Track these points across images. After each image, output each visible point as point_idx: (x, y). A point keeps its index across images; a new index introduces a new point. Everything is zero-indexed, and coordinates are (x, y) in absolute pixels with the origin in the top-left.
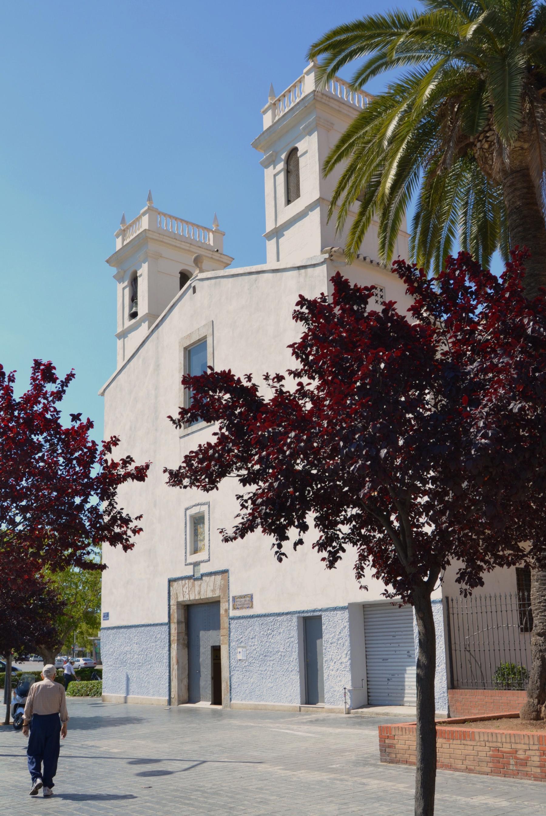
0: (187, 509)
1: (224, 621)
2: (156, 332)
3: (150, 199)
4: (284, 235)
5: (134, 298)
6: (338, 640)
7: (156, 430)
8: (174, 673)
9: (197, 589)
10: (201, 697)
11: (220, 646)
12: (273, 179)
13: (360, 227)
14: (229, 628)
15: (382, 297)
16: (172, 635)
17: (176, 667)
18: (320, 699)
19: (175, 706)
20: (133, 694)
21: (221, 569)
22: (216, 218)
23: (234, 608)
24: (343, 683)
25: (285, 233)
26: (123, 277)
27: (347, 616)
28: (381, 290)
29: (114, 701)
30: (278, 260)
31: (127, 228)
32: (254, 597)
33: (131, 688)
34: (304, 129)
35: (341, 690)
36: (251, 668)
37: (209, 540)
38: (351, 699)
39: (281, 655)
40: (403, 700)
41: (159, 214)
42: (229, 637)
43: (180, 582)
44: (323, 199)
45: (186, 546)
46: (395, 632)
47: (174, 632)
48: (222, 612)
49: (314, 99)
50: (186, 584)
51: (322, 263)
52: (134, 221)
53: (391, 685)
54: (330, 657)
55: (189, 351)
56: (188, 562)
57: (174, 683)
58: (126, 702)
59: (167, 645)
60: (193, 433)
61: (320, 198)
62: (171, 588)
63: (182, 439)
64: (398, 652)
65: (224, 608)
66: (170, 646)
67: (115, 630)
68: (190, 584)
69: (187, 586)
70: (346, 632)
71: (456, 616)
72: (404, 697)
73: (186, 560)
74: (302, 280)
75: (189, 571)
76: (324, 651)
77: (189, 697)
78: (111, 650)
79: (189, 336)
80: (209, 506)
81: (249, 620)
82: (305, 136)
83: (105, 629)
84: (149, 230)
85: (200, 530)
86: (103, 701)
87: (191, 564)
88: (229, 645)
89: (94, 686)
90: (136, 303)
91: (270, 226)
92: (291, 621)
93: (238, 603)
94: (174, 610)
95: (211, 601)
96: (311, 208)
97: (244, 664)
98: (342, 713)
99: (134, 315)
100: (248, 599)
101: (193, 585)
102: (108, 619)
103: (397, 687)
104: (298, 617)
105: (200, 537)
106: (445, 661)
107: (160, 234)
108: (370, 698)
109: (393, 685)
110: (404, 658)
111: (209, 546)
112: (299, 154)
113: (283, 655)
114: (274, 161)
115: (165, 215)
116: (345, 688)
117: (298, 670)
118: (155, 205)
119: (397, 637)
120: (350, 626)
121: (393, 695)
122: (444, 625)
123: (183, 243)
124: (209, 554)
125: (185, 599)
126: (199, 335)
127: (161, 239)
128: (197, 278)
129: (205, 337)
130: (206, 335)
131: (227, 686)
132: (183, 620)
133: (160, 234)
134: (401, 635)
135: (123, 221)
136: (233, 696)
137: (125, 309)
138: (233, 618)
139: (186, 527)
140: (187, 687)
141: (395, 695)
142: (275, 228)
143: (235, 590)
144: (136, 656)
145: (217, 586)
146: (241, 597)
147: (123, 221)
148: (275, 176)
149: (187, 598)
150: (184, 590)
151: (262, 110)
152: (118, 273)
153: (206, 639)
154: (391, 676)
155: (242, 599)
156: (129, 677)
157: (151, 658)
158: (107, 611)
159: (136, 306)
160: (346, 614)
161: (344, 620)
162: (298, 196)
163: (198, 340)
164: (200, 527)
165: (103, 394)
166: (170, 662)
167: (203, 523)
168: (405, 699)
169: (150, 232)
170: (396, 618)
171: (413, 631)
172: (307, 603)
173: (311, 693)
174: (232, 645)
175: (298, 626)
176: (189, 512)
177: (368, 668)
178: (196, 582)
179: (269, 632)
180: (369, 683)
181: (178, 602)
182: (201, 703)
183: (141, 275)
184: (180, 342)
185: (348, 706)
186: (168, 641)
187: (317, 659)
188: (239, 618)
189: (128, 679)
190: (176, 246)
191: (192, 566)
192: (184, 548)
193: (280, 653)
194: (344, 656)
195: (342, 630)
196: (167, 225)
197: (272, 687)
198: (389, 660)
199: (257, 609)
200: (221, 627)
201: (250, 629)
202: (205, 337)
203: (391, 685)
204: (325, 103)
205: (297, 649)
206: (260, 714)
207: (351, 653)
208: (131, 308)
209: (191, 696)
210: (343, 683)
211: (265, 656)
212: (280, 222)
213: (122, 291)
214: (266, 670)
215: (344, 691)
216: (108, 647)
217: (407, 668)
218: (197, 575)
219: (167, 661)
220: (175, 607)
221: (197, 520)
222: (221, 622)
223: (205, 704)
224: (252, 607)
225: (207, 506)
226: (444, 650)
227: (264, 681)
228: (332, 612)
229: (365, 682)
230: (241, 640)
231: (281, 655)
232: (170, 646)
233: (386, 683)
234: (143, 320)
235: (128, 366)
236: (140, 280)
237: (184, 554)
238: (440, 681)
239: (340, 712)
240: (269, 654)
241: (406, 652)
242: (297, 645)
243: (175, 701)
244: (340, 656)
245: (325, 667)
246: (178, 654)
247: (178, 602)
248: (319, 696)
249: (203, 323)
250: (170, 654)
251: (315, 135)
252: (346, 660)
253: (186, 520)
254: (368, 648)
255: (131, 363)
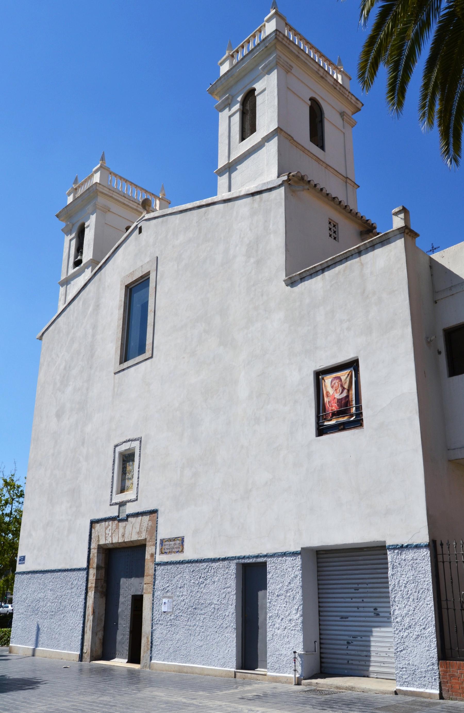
0: (116, 446)
1: (149, 567)
2: (99, 274)
3: (103, 159)
4: (237, 169)
5: (79, 249)
6: (287, 591)
7: (91, 368)
8: (89, 624)
9: (121, 530)
10: (117, 653)
11: (142, 596)
12: (228, 121)
13: (376, 46)
14: (155, 575)
15: (335, 232)
16: (89, 581)
17: (91, 618)
18: (259, 664)
19: (86, 663)
20: (41, 647)
21: (149, 509)
22: (163, 188)
23: (162, 553)
24: (291, 645)
25: (238, 167)
26: (71, 230)
27: (300, 563)
28: (334, 226)
29: (21, 654)
30: (230, 190)
31: (79, 187)
32: (185, 540)
33: (41, 640)
34: (263, 68)
35: (289, 653)
36: (177, 622)
37: (138, 478)
38: (302, 666)
39: (214, 608)
40: (368, 670)
41: (110, 173)
42: (154, 585)
43: (103, 523)
44: (281, 130)
45: (112, 485)
46: (358, 584)
47: (92, 578)
48: (147, 556)
49: (276, 38)
50: (109, 525)
51: (280, 186)
52: (86, 179)
53: (352, 650)
54: (276, 612)
55: (131, 290)
56: (113, 501)
57: (88, 636)
58: (33, 655)
59: (84, 592)
60: (128, 368)
61: (278, 127)
62: (93, 530)
63: (116, 375)
64: (361, 609)
65: (150, 553)
66: (86, 593)
67: (30, 575)
68: (114, 525)
69: (110, 527)
70: (298, 582)
71: (447, 565)
72: (369, 666)
73: (111, 499)
74: (256, 205)
75: (114, 512)
76: (268, 604)
77: (103, 652)
78: (24, 596)
79: (132, 274)
80: (141, 442)
81: (178, 566)
82: (264, 75)
83: (19, 573)
84: (100, 184)
85: (129, 468)
86: (10, 652)
87: (116, 504)
88: (153, 595)
89: (5, 634)
90: (82, 253)
91: (222, 162)
92: (228, 568)
93: (167, 547)
94: (94, 554)
95: (135, 545)
96: (268, 139)
97: (168, 617)
98: (290, 683)
99: (77, 263)
100: (178, 542)
101: (117, 527)
102: (24, 563)
103: (359, 653)
104: (237, 564)
105: (128, 476)
106: (434, 622)
107: (110, 189)
108: (323, 665)
109: (354, 650)
110: (369, 617)
111: (138, 484)
112: (256, 93)
113: (216, 608)
114: (230, 104)
115: (116, 175)
116: (295, 652)
117: (235, 627)
118: (106, 165)
119: (360, 590)
120: (303, 575)
121: (354, 662)
122: (432, 575)
123: (131, 202)
124: (137, 493)
125: (107, 542)
126: (142, 272)
127: (111, 195)
128: (144, 219)
129: (148, 273)
130: (149, 272)
131: (148, 642)
132: (103, 566)
133: (110, 189)
134: (366, 588)
135: (76, 181)
136: (154, 654)
137: (70, 259)
138: (159, 564)
139: (114, 464)
140: (102, 641)
141: (357, 663)
142: (228, 163)
143: (164, 532)
144: (49, 604)
145: (144, 528)
146: (170, 540)
147: (76, 181)
148: (230, 117)
149: (109, 541)
150: (107, 532)
151: (220, 62)
152: (67, 225)
153: (127, 587)
154: (351, 638)
155: (171, 543)
156: (40, 626)
157: (65, 607)
158: (23, 555)
159: (82, 255)
160: (298, 561)
161: (295, 568)
162: (253, 130)
163: (141, 277)
164: (129, 465)
165: (41, 338)
166: (85, 612)
167: (133, 460)
168: (371, 669)
169: (101, 186)
170: (359, 567)
171: (388, 583)
172: (248, 548)
173: (250, 655)
174: (156, 594)
175: (237, 574)
176: (118, 449)
177: (322, 627)
178: (120, 524)
179: (201, 580)
180: (322, 646)
181: (99, 545)
182: (116, 660)
183: (88, 226)
184: (122, 281)
185: (297, 676)
186: (85, 588)
187: (257, 614)
188: (167, 563)
189: (38, 629)
190: (124, 204)
191: (118, 506)
192: (111, 486)
193: (213, 606)
194: (294, 612)
195: (292, 580)
196: (116, 184)
197: (202, 646)
198: (350, 619)
199: (188, 554)
200: (145, 574)
201: (179, 576)
202: (148, 273)
203: (352, 650)
204: (285, 45)
205: (234, 602)
206: (187, 681)
207: (303, 608)
208: (76, 257)
209: (105, 650)
210: (291, 645)
211: (195, 609)
212: (233, 158)
213: (69, 243)
214: (195, 625)
215: (293, 656)
216: (21, 593)
217: (374, 629)
218: (123, 516)
219: (82, 610)
220: (96, 551)
221: (126, 457)
222: (146, 568)
223: (120, 663)
224: (182, 551)
225: (138, 442)
226: (433, 608)
227: (192, 638)
228: (280, 559)
229: (317, 644)
230: (168, 589)
231: (214, 608)
232: (86, 593)
233: (345, 647)
234: (87, 266)
235: (68, 309)
236: (87, 231)
237: (110, 494)
238: (427, 649)
239: (287, 681)
240: (199, 606)
241: (372, 609)
242: (235, 596)
243: (87, 656)
244: (289, 612)
245: (268, 625)
246: (95, 603)
247: (99, 545)
248: (259, 659)
249: (147, 259)
250: (85, 603)
251: (274, 74)
252: (297, 617)
253: (114, 457)
254: (322, 602)
255: (71, 306)
